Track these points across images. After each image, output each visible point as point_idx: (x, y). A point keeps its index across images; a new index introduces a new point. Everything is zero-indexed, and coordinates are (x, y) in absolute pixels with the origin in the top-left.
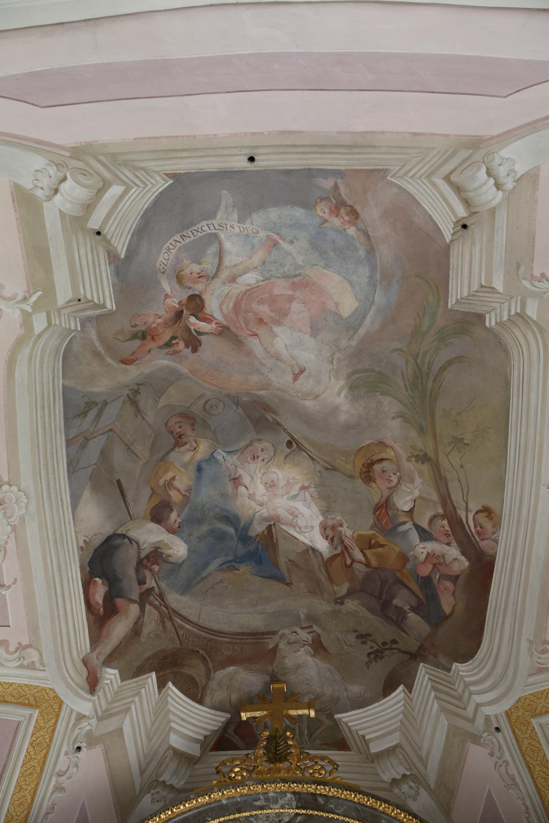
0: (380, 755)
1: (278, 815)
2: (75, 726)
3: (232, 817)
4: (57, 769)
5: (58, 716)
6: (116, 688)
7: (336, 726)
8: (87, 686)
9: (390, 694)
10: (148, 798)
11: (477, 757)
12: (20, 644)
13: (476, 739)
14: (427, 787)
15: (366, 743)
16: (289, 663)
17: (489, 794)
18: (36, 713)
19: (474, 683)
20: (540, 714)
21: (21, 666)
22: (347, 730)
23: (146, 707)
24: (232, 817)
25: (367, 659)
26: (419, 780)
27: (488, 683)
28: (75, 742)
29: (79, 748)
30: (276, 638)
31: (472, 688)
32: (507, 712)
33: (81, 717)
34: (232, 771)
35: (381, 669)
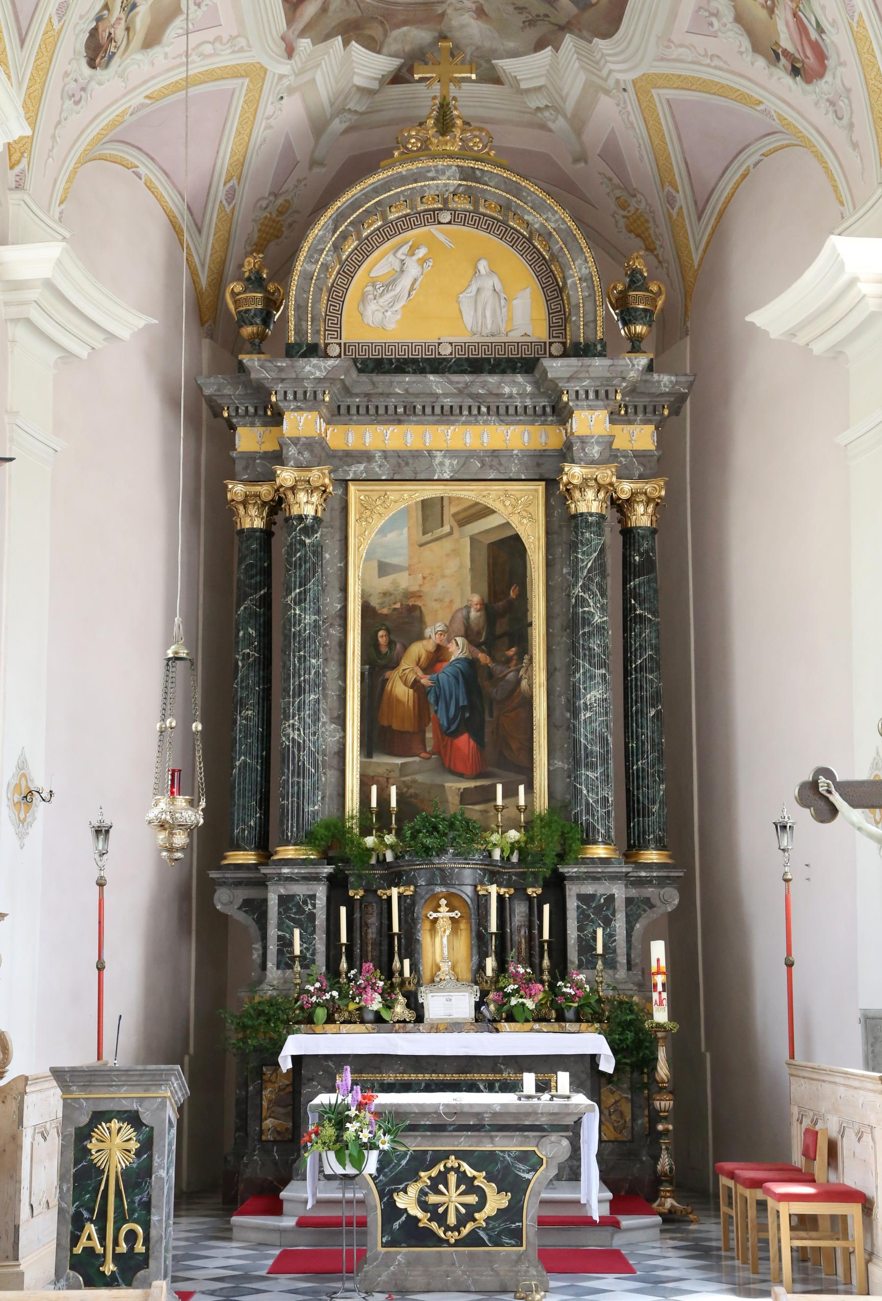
0: (527, 91)
1: (445, 185)
2: (277, 84)
3: (411, 186)
4: (266, 115)
5: (264, 79)
6: (308, 51)
7: (493, 68)
8: (285, 55)
9: (540, 51)
10: (337, 120)
11: (606, 105)
12: (231, 36)
13: (607, 92)
14: (565, 116)
15: (518, 81)
16: (455, 23)
17: (613, 131)
18: (247, 81)
19: (609, 55)
20: (659, 87)
21: (233, 52)
22: (502, 71)
23: (334, 61)
24: (411, 186)
25: (522, 25)
26: (558, 110)
27: (622, 57)
28: (278, 94)
29: (282, 98)
30: (445, 6)
31: (608, 58)
32: (633, 81)
33: (282, 77)
34: (409, 142)
35: (533, 34)
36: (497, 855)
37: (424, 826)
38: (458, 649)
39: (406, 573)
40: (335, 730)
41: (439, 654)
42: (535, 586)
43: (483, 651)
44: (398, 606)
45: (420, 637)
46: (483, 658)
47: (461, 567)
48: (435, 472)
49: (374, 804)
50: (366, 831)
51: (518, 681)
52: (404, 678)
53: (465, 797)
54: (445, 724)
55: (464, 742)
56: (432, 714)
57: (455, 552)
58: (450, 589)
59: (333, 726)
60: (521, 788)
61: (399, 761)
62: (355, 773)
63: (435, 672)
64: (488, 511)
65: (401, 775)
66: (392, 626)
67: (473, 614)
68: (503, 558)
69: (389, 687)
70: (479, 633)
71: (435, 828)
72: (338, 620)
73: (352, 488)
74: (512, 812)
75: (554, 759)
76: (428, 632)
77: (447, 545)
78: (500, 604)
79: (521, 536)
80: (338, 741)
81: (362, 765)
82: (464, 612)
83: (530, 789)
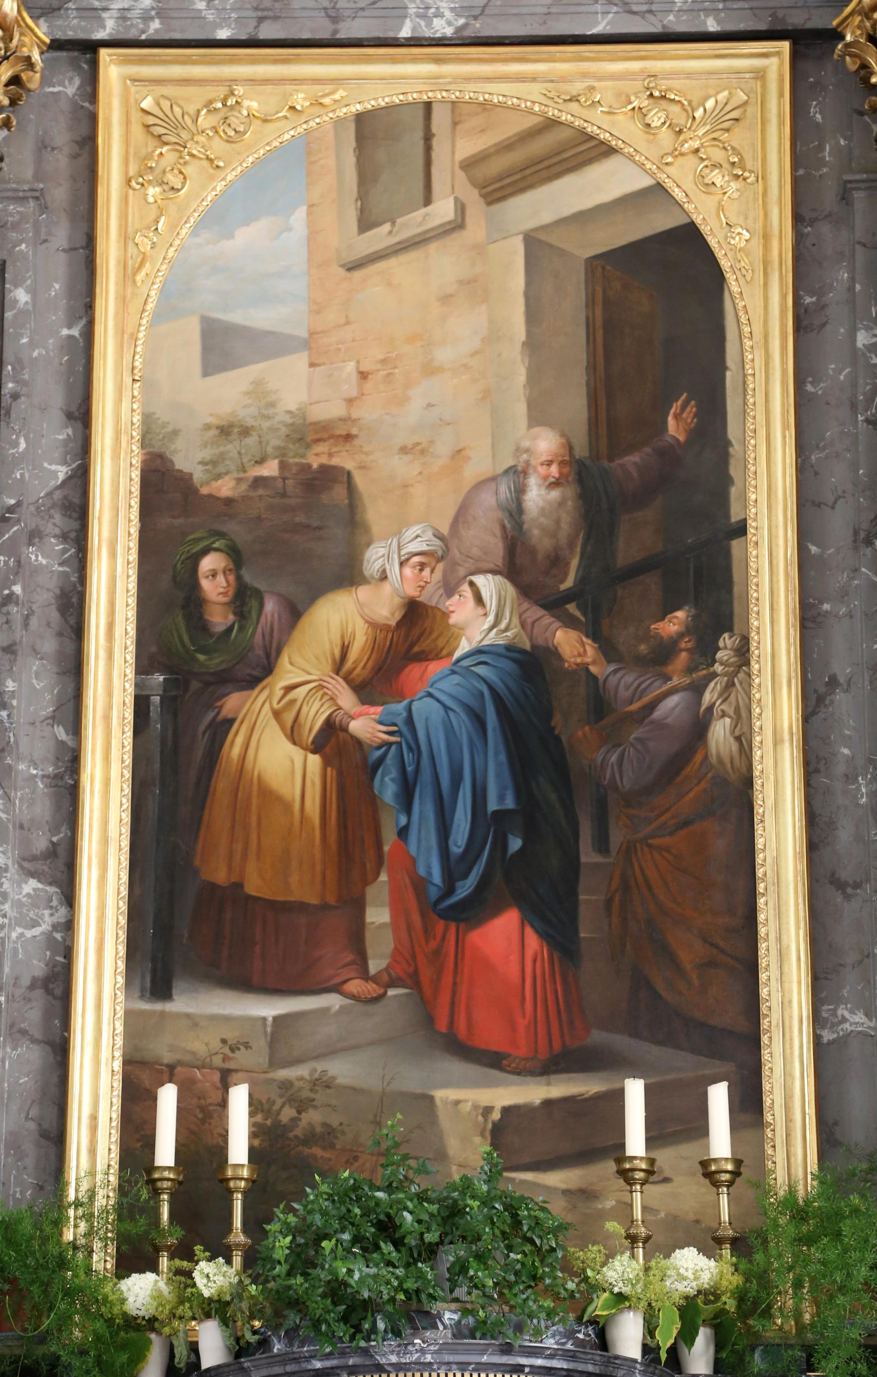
36: (629, 1337)
37: (346, 1220)
38: (482, 617)
39: (299, 361)
40: (35, 899)
41: (414, 631)
42: (755, 399)
43: (570, 622)
44: (270, 469)
45: (349, 575)
46: (570, 644)
47: (494, 336)
48: (401, 13)
49: (165, 1153)
50: (134, 1258)
51: (700, 727)
52: (289, 717)
53: (508, 1132)
54: (437, 877)
55: (505, 938)
56: (389, 838)
57: (475, 289)
58: (453, 414)
59: (32, 885)
60: (718, 1096)
61: (268, 1008)
62: (105, 1054)
63: (400, 696)
64: (592, 150)
65: (275, 1062)
66: (242, 545)
67: (537, 496)
68: (649, 303)
69: (234, 747)
70: (557, 561)
71: (388, 1227)
72: (58, 518)
73: (112, 68)
74: (685, 1194)
75: (839, 1001)
76: (375, 557)
77: (444, 264)
78: (634, 458)
79: (705, 229)
80: (49, 937)
81: (134, 1024)
82: (504, 490)
83: (749, 1106)
